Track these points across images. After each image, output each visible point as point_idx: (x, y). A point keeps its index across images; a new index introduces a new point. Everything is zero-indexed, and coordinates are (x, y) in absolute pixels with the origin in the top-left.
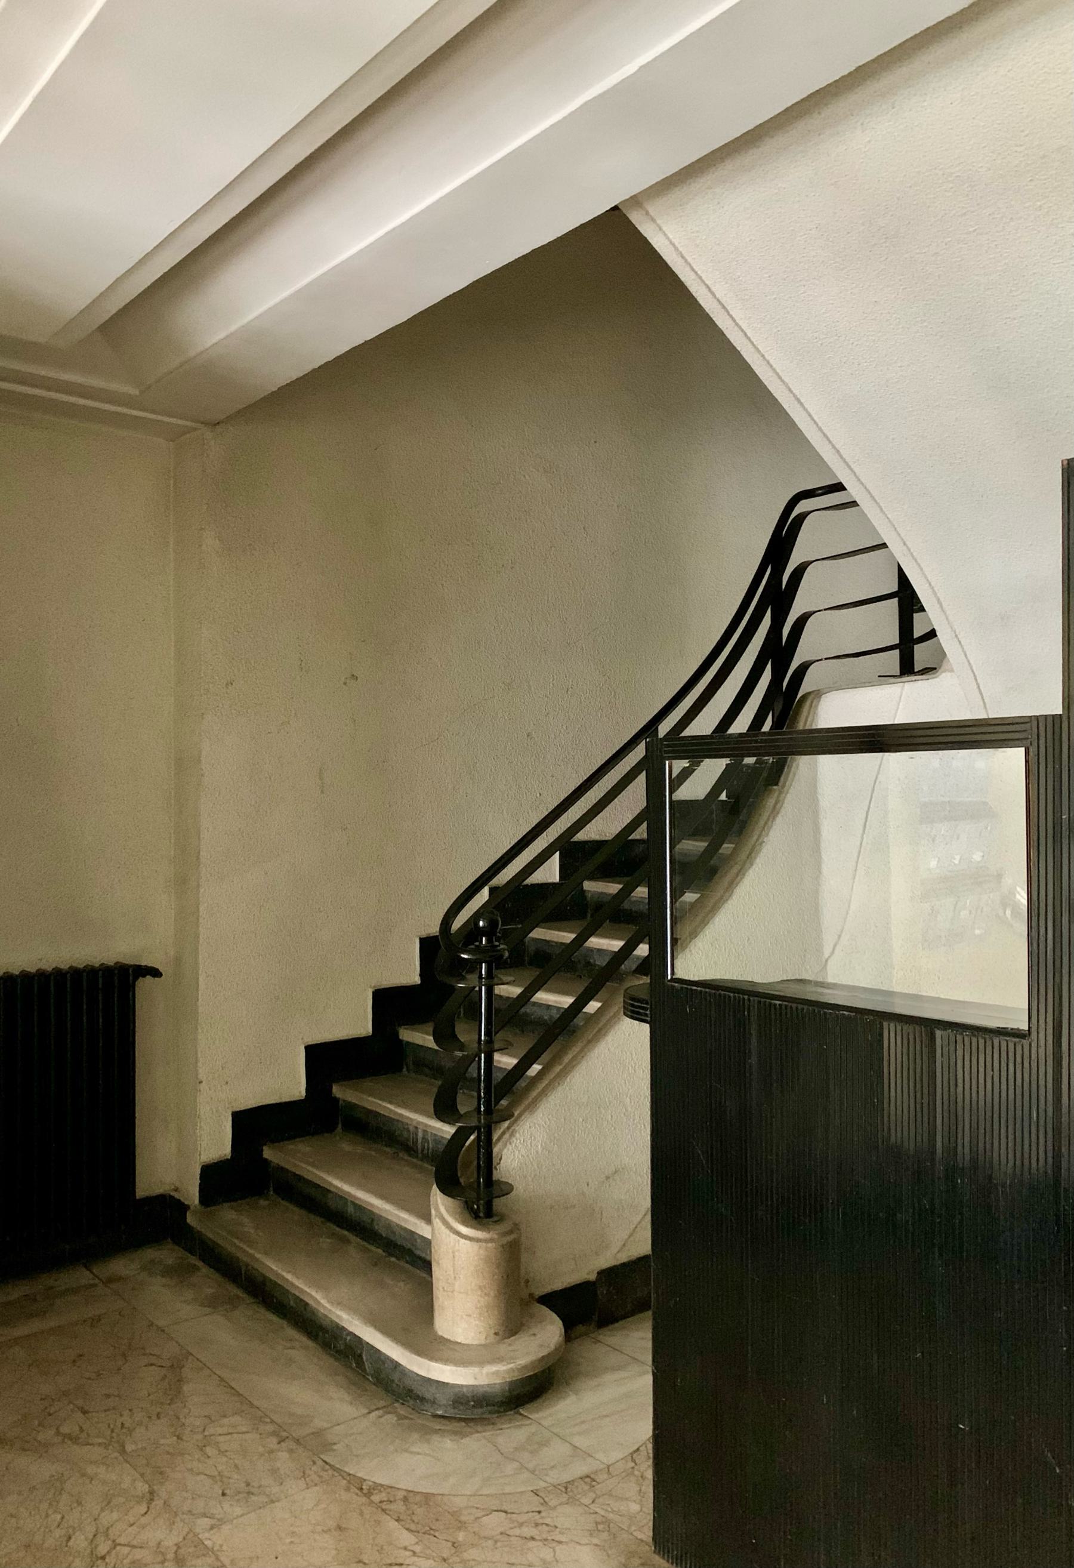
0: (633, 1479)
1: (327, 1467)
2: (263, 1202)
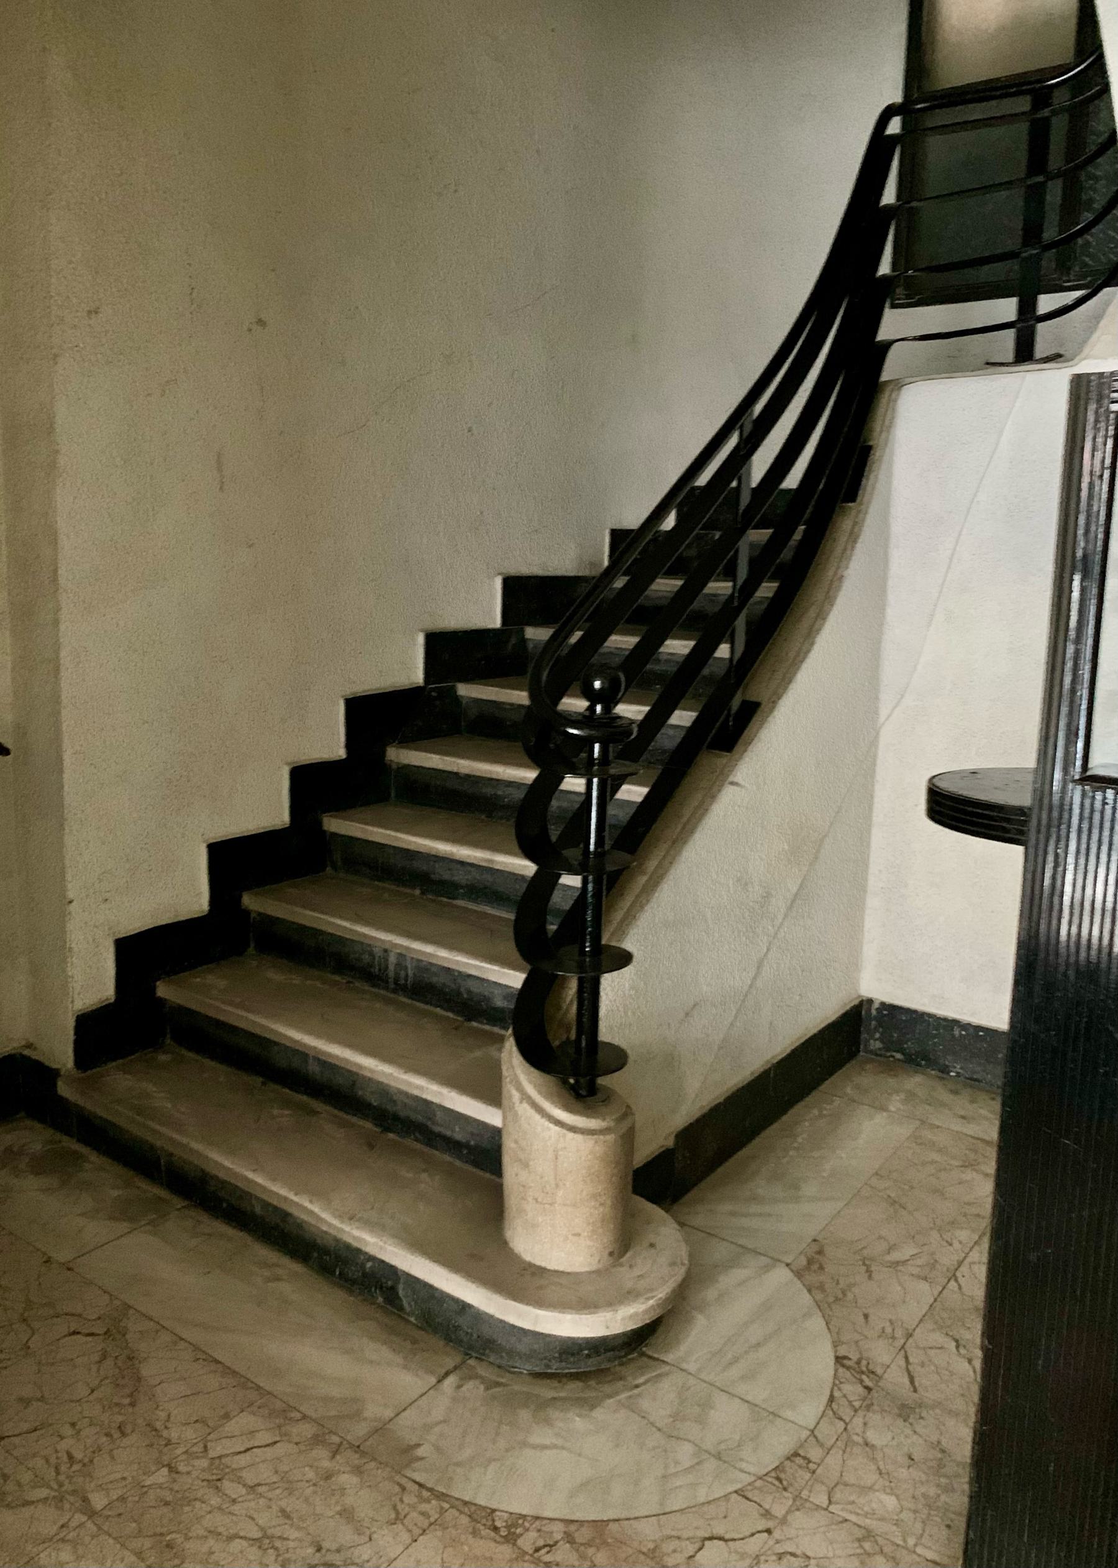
0: (857, 1450)
1: (426, 1494)
2: (163, 1058)
